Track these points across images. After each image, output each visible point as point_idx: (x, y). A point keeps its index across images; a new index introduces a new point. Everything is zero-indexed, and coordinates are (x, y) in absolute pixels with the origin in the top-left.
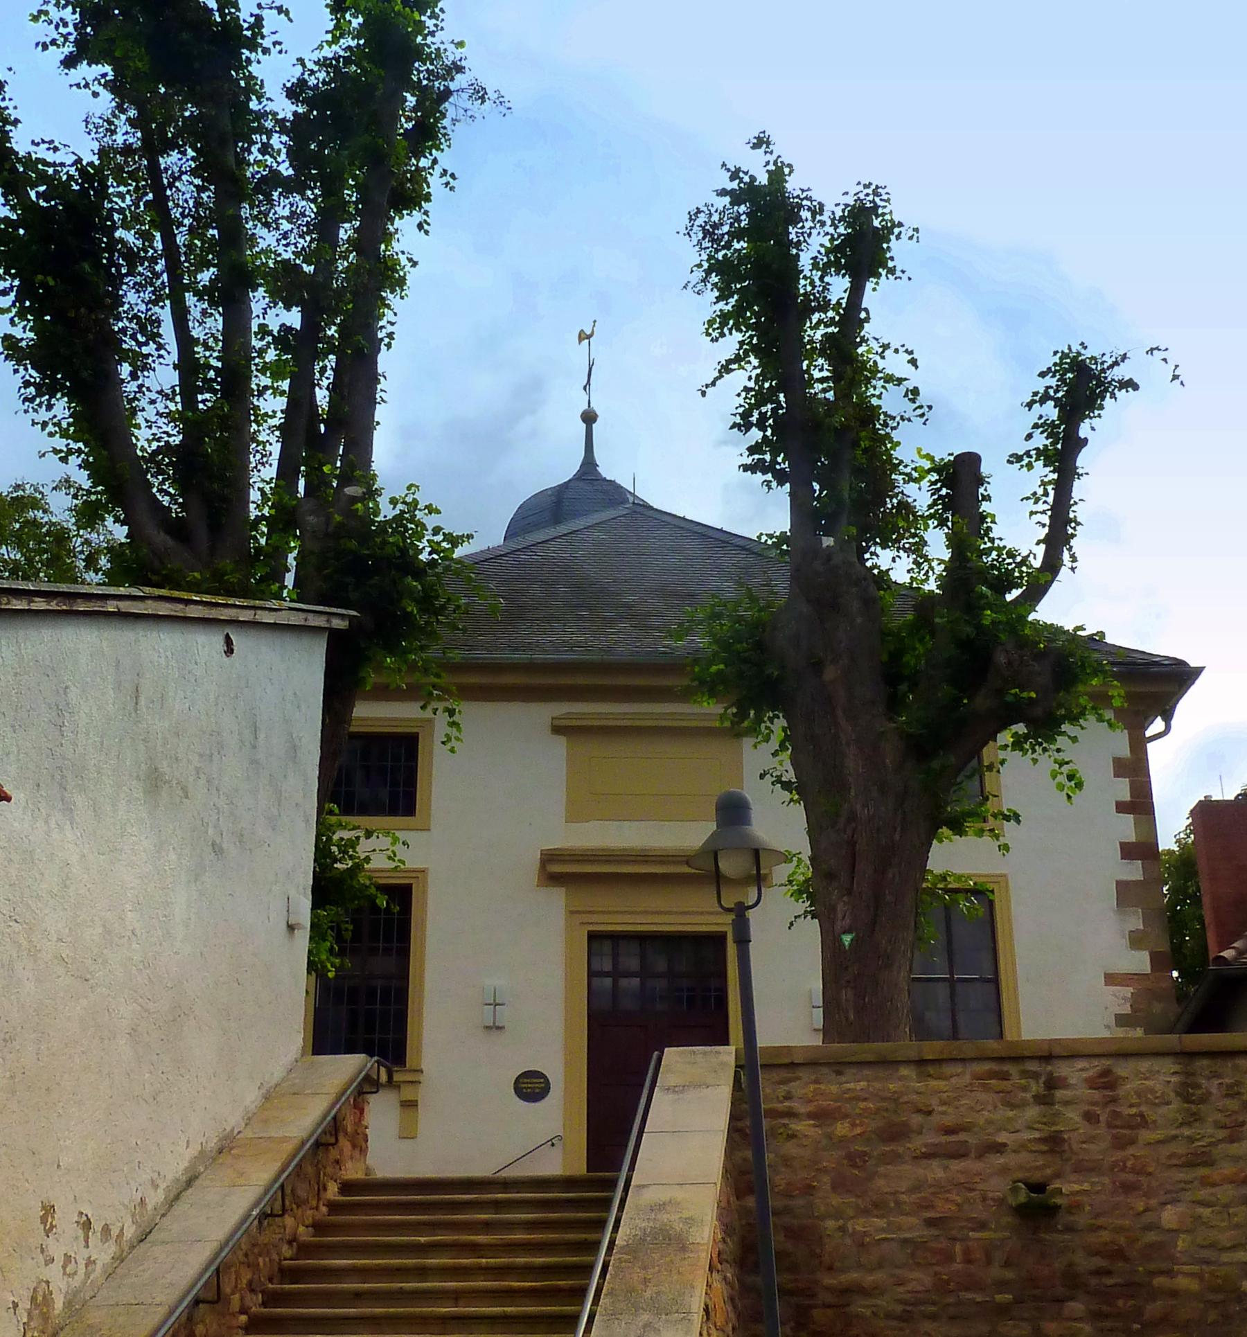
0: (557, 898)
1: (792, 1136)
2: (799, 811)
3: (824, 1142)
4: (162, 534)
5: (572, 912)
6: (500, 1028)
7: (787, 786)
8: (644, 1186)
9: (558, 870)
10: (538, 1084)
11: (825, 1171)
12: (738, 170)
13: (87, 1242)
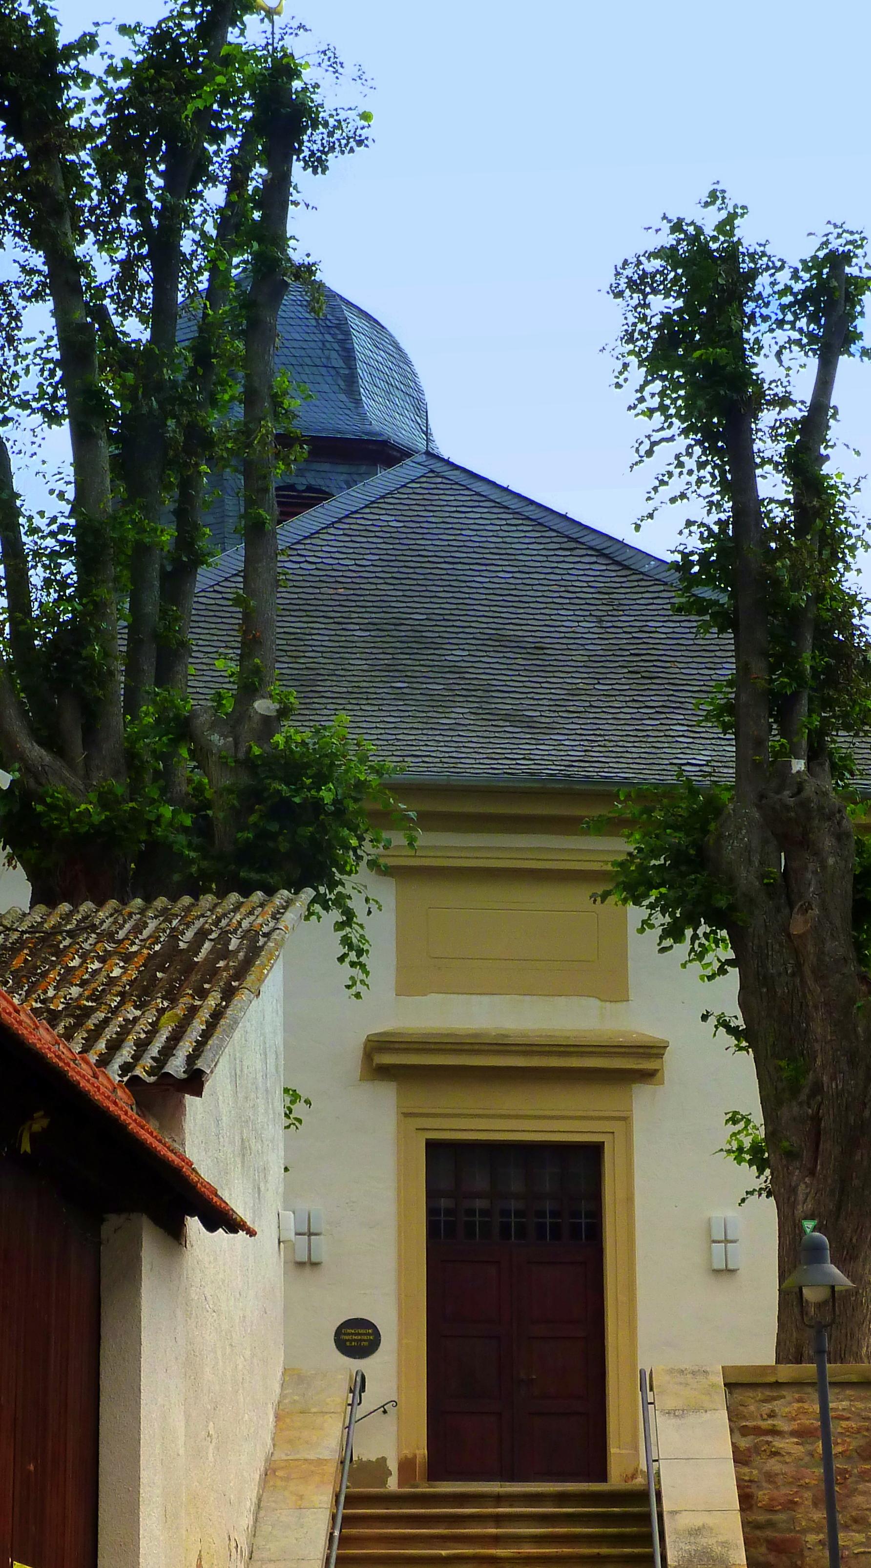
0: (385, 1100)
1: (776, 1454)
2: (747, 1061)
3: (807, 1459)
4: (37, 747)
5: (406, 1115)
6: (315, 1265)
7: (732, 1031)
8: (676, 1512)
9: (391, 1062)
10: (366, 1336)
11: (806, 1487)
12: (680, 221)
13: (200, 1558)
